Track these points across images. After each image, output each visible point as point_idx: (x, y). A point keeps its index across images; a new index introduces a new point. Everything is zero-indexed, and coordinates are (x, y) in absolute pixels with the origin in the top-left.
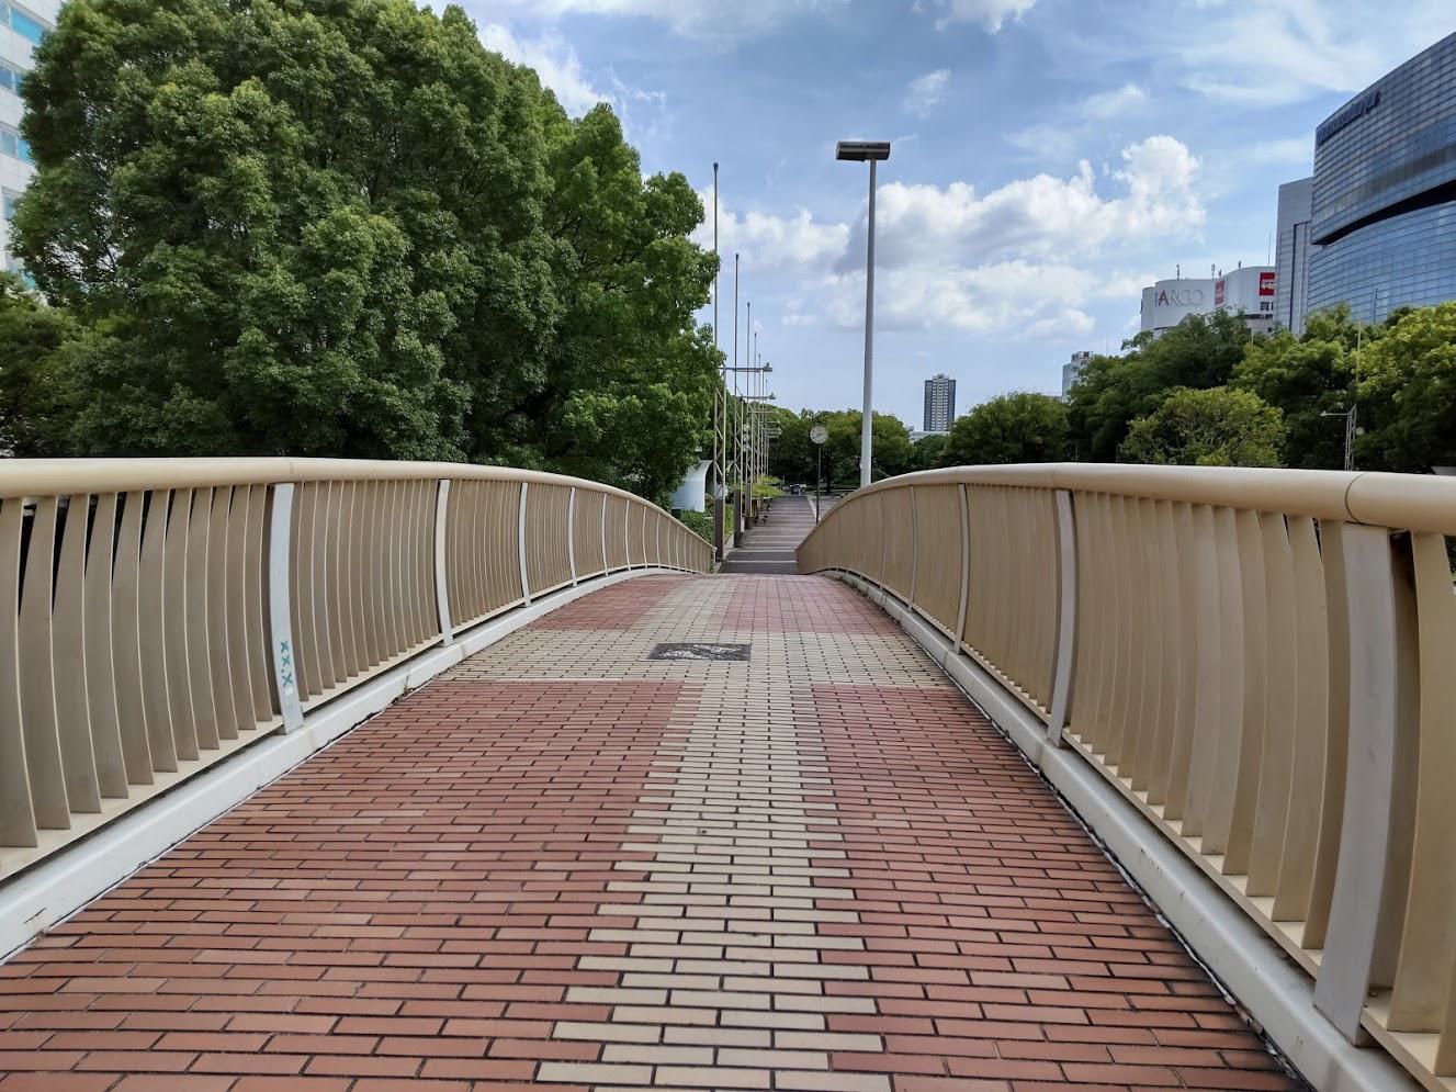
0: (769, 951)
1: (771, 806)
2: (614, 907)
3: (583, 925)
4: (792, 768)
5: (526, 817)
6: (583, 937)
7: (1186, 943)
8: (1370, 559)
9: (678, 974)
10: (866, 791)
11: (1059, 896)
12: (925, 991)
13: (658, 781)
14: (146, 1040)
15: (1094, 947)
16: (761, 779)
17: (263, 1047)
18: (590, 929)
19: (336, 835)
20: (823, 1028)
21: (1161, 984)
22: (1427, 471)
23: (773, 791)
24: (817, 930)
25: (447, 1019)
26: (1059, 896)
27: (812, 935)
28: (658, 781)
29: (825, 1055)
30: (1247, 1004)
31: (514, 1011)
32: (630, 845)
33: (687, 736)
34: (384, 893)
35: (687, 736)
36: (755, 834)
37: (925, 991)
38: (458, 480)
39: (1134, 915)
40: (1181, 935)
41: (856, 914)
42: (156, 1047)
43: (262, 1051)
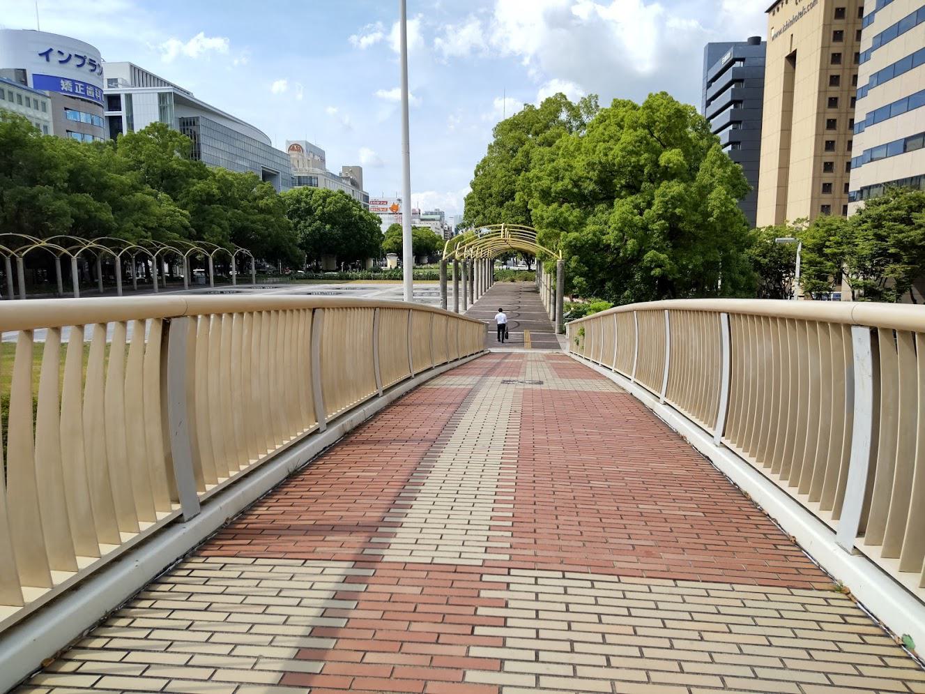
0: (511, 566)
2: (363, 616)
9: (450, 605)
12: (624, 595)
14: (143, 634)
15: (832, 685)
16: (445, 508)
17: (213, 635)
20: (569, 650)
22: (647, 301)
24: (537, 633)
27: (533, 601)
29: (576, 650)
30: (737, 483)
32: (370, 550)
34: (194, 600)
37: (624, 595)
38: (671, 310)
41: (561, 573)
42: (124, 660)
43: (186, 665)
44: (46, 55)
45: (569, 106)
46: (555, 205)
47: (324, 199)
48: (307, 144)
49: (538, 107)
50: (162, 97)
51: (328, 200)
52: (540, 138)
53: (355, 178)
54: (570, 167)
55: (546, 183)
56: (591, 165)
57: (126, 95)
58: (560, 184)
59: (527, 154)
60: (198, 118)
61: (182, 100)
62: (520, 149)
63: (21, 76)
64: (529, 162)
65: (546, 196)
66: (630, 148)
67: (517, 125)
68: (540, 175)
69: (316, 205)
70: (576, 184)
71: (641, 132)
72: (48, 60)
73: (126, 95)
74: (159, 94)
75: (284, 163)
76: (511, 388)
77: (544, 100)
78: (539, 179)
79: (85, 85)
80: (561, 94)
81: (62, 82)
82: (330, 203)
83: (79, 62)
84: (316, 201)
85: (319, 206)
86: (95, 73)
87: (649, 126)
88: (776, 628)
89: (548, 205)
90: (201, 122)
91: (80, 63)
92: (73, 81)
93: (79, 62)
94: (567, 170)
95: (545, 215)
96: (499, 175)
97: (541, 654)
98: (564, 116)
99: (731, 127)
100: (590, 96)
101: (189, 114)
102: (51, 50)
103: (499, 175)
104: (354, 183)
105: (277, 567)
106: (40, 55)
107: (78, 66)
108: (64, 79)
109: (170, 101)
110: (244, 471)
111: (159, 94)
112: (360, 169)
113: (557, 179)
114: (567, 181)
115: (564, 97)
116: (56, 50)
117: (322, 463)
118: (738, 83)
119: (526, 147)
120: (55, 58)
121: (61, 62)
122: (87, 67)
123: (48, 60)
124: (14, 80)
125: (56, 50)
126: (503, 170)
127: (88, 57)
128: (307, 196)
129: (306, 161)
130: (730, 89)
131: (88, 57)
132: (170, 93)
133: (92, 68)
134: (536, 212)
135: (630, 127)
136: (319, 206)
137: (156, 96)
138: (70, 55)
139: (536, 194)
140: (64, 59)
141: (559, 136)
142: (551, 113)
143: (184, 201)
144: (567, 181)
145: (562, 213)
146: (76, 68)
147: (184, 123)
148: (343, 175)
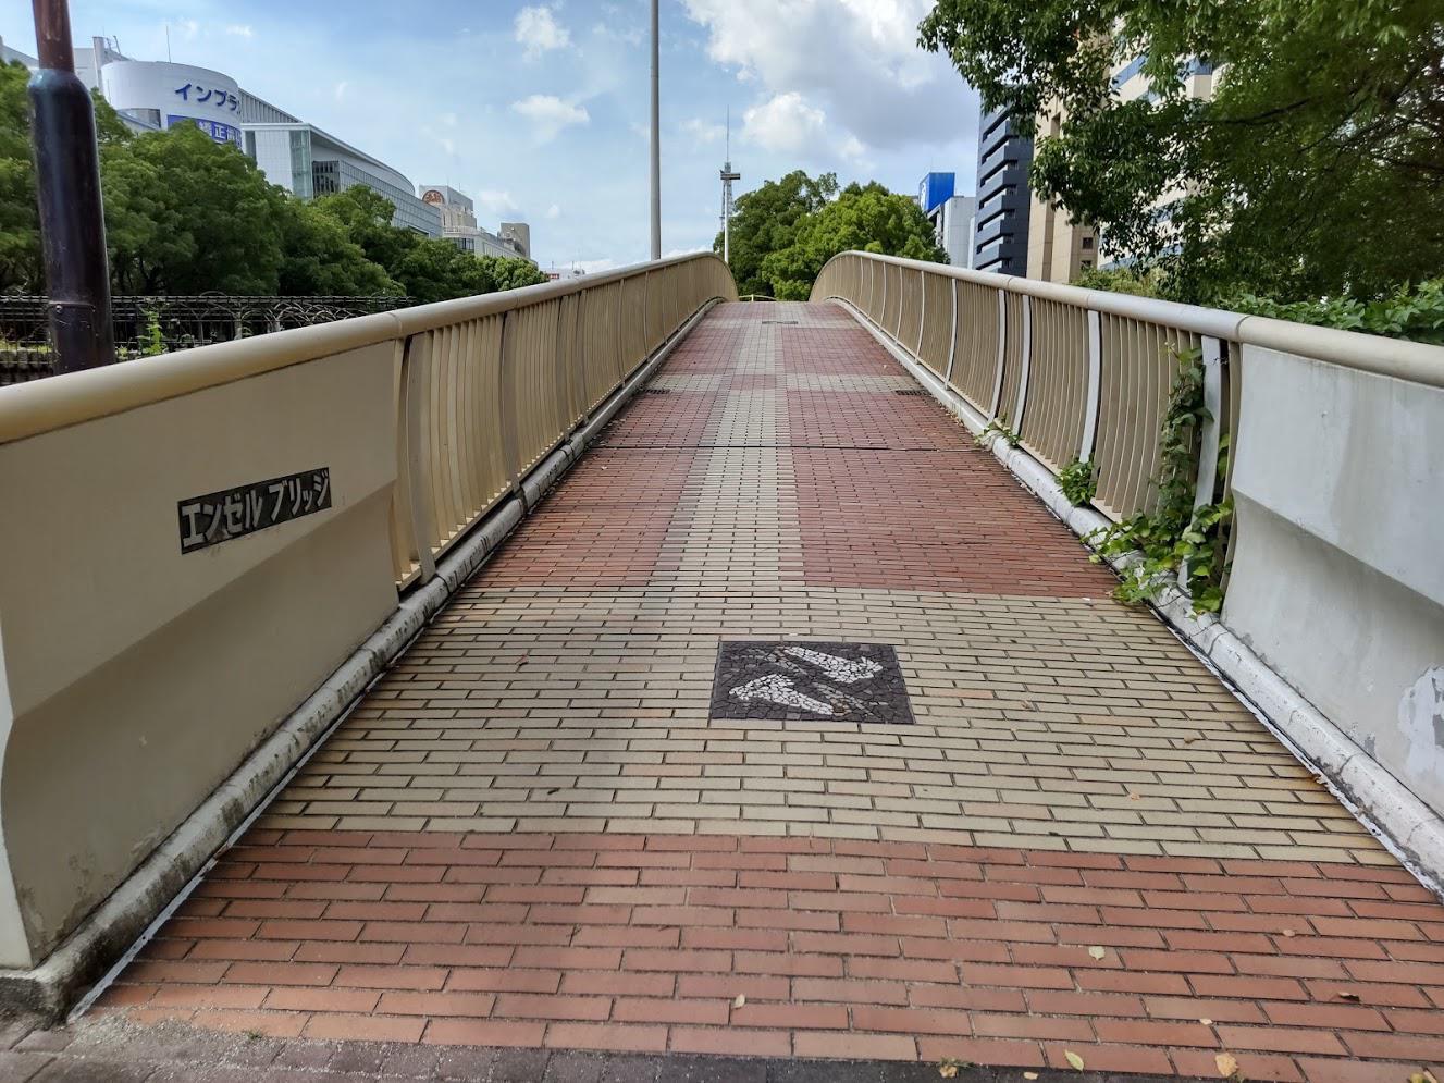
1: (781, 602)
3: (511, 814)
4: (798, 600)
5: (363, 789)
6: (494, 861)
7: (1238, 690)
8: (1211, 350)
10: (945, 759)
11: (1349, 964)
13: (675, 534)
18: (537, 775)
19: (391, 754)
21: (1313, 821)
23: (791, 772)
25: (395, 803)
26: (1259, 849)
28: (675, 534)
31: (534, 694)
33: (682, 546)
35: (682, 546)
36: (768, 612)
39: (1251, 732)
40: (1263, 713)
44: (184, 91)
45: (809, 183)
46: (791, 281)
47: (511, 271)
48: (451, 191)
49: (778, 183)
50: (295, 136)
51: (517, 272)
52: (780, 216)
53: (519, 240)
54: (804, 252)
55: (784, 264)
56: (818, 251)
57: (247, 132)
58: (795, 265)
59: (768, 233)
60: (336, 163)
61: (319, 140)
62: (762, 227)
63: (155, 117)
64: (770, 240)
65: (785, 274)
66: (844, 240)
67: (758, 202)
68: (780, 257)
69: (501, 279)
70: (807, 265)
71: (854, 228)
72: (185, 98)
73: (247, 132)
74: (292, 132)
75: (435, 221)
76: (772, 327)
77: (784, 177)
78: (779, 261)
79: (226, 127)
80: (801, 171)
81: (201, 124)
82: (519, 277)
83: (219, 99)
84: (501, 274)
85: (505, 279)
86: (235, 112)
87: (860, 226)
88: (1041, 823)
89: (787, 281)
90: (341, 167)
91: (220, 101)
92: (213, 123)
93: (219, 99)
94: (800, 254)
95: (784, 288)
96: (742, 252)
97: (748, 756)
98: (804, 192)
99: (1004, 192)
100: (829, 174)
101: (325, 157)
102: (189, 86)
103: (742, 252)
104: (518, 248)
105: (367, 790)
106: (177, 92)
107: (219, 104)
108: (204, 121)
109: (305, 142)
110: (406, 580)
111: (292, 132)
112: (526, 228)
113: (793, 261)
114: (800, 263)
115: (804, 174)
116: (194, 85)
117: (503, 565)
118: (1012, 140)
119: (767, 225)
120: (193, 95)
121: (200, 100)
122: (228, 105)
123: (185, 98)
124: (147, 120)
125: (194, 85)
126: (745, 247)
127: (229, 93)
128: (488, 267)
129: (456, 217)
130: (1003, 146)
131: (229, 93)
132: (306, 132)
133: (231, 106)
134: (777, 287)
135: (846, 224)
136: (505, 279)
137: (288, 134)
138: (210, 92)
139: (777, 273)
140: (203, 96)
141: (798, 214)
142: (790, 191)
143: (397, 272)
144: (800, 263)
145: (796, 288)
146: (215, 107)
147: (317, 169)
148: (504, 237)
